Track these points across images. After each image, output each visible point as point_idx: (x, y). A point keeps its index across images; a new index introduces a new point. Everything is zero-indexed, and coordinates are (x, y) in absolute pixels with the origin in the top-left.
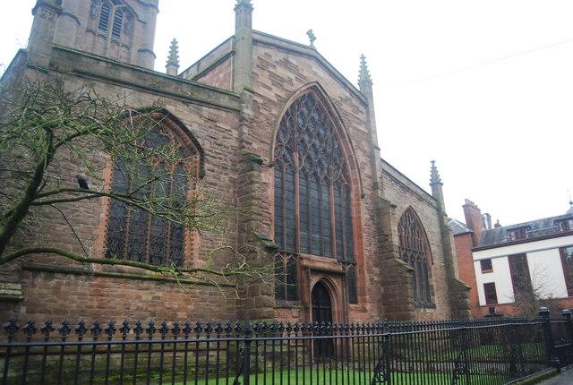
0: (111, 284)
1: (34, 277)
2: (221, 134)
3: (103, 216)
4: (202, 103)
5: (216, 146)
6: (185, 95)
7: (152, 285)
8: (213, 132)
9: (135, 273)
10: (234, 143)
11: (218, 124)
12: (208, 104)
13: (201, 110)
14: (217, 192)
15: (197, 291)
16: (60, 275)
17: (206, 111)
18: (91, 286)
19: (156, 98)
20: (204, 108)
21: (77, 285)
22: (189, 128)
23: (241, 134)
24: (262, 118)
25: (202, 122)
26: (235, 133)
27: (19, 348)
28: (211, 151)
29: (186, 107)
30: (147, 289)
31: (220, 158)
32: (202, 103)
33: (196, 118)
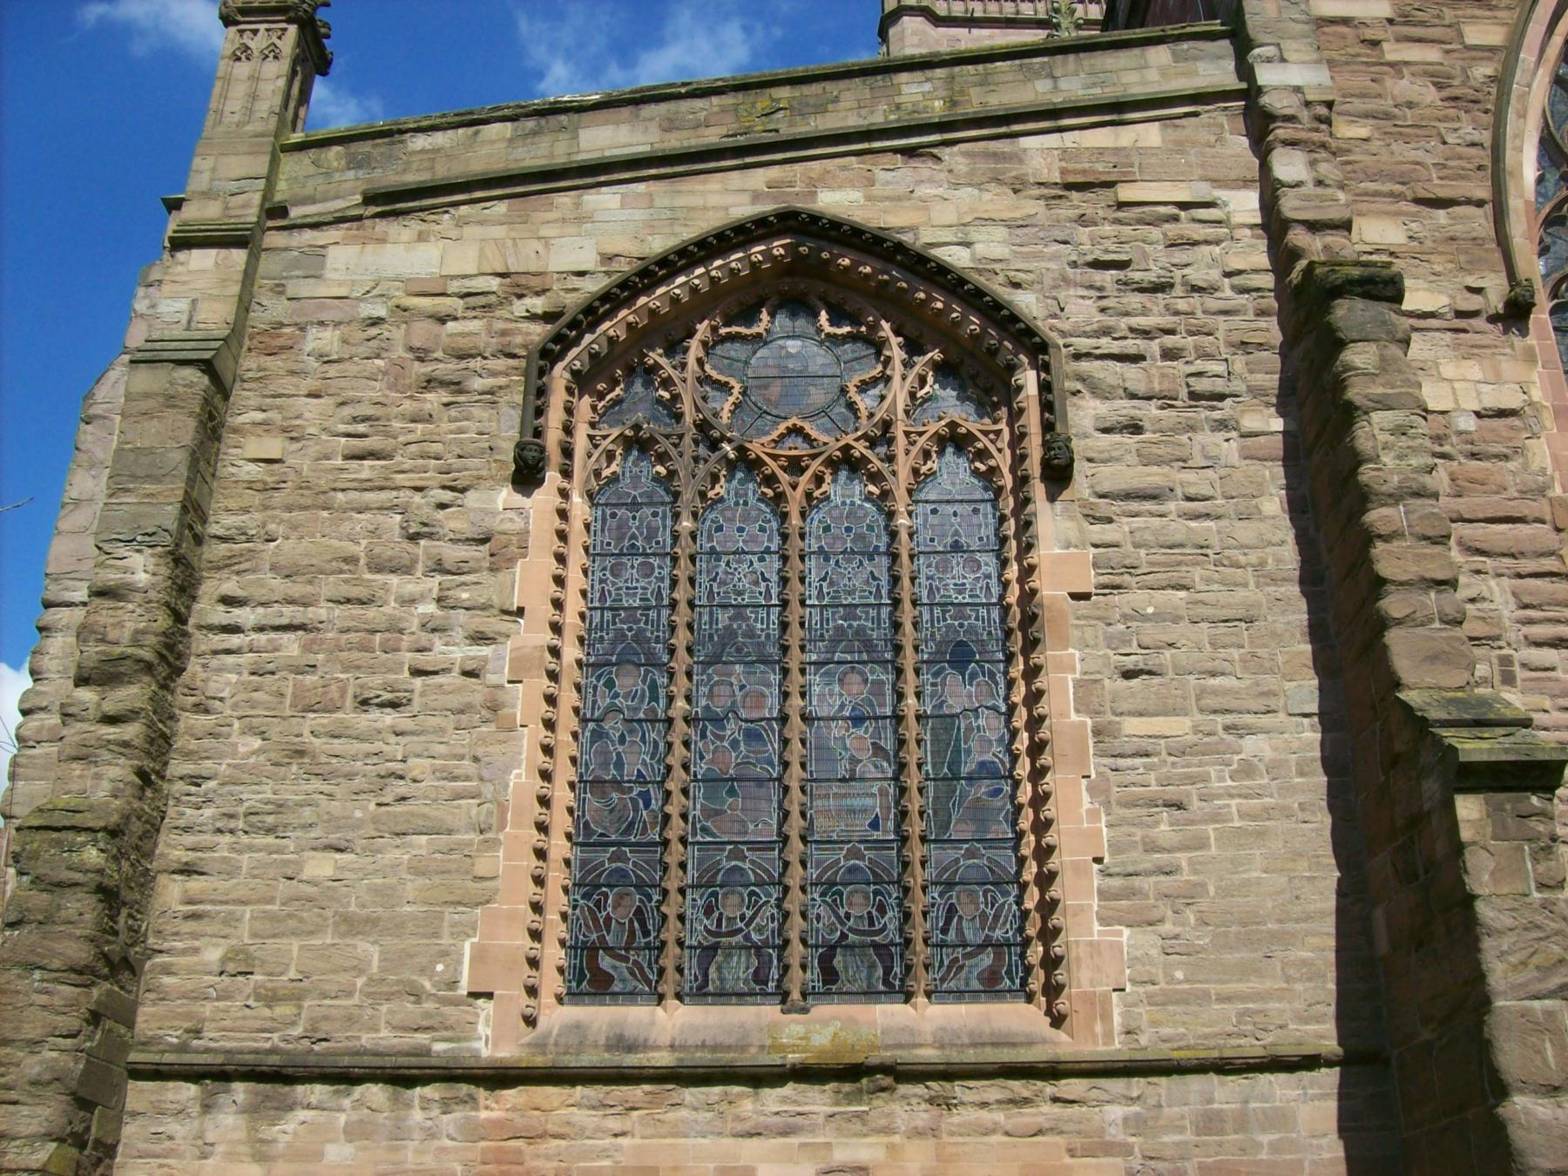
0: (581, 1116)
1: (207, 1108)
2: (1155, 233)
3: (521, 779)
4: (1006, 122)
5: (1135, 300)
6: (924, 117)
7: (818, 1100)
8: (1103, 238)
9: (408, 1054)
10: (1254, 255)
11: (1126, 193)
12: (1051, 116)
13: (1018, 157)
14: (1179, 529)
15: (1116, 1112)
16: (318, 1092)
17: (1040, 153)
18: (474, 1132)
19: (758, 178)
20: (1025, 142)
21: (399, 1134)
22: (957, 258)
23: (1270, 191)
24: (1404, 87)
25: (1038, 208)
26: (1245, 205)
27: (879, 116)
28: (1106, 332)
29: (924, 168)
30: (785, 1132)
31: (1169, 354)
32: (1006, 122)
33: (997, 201)
